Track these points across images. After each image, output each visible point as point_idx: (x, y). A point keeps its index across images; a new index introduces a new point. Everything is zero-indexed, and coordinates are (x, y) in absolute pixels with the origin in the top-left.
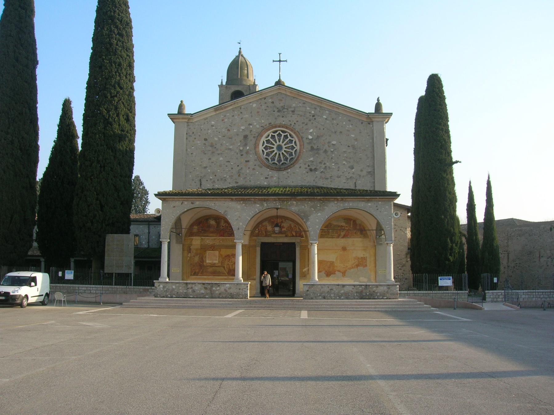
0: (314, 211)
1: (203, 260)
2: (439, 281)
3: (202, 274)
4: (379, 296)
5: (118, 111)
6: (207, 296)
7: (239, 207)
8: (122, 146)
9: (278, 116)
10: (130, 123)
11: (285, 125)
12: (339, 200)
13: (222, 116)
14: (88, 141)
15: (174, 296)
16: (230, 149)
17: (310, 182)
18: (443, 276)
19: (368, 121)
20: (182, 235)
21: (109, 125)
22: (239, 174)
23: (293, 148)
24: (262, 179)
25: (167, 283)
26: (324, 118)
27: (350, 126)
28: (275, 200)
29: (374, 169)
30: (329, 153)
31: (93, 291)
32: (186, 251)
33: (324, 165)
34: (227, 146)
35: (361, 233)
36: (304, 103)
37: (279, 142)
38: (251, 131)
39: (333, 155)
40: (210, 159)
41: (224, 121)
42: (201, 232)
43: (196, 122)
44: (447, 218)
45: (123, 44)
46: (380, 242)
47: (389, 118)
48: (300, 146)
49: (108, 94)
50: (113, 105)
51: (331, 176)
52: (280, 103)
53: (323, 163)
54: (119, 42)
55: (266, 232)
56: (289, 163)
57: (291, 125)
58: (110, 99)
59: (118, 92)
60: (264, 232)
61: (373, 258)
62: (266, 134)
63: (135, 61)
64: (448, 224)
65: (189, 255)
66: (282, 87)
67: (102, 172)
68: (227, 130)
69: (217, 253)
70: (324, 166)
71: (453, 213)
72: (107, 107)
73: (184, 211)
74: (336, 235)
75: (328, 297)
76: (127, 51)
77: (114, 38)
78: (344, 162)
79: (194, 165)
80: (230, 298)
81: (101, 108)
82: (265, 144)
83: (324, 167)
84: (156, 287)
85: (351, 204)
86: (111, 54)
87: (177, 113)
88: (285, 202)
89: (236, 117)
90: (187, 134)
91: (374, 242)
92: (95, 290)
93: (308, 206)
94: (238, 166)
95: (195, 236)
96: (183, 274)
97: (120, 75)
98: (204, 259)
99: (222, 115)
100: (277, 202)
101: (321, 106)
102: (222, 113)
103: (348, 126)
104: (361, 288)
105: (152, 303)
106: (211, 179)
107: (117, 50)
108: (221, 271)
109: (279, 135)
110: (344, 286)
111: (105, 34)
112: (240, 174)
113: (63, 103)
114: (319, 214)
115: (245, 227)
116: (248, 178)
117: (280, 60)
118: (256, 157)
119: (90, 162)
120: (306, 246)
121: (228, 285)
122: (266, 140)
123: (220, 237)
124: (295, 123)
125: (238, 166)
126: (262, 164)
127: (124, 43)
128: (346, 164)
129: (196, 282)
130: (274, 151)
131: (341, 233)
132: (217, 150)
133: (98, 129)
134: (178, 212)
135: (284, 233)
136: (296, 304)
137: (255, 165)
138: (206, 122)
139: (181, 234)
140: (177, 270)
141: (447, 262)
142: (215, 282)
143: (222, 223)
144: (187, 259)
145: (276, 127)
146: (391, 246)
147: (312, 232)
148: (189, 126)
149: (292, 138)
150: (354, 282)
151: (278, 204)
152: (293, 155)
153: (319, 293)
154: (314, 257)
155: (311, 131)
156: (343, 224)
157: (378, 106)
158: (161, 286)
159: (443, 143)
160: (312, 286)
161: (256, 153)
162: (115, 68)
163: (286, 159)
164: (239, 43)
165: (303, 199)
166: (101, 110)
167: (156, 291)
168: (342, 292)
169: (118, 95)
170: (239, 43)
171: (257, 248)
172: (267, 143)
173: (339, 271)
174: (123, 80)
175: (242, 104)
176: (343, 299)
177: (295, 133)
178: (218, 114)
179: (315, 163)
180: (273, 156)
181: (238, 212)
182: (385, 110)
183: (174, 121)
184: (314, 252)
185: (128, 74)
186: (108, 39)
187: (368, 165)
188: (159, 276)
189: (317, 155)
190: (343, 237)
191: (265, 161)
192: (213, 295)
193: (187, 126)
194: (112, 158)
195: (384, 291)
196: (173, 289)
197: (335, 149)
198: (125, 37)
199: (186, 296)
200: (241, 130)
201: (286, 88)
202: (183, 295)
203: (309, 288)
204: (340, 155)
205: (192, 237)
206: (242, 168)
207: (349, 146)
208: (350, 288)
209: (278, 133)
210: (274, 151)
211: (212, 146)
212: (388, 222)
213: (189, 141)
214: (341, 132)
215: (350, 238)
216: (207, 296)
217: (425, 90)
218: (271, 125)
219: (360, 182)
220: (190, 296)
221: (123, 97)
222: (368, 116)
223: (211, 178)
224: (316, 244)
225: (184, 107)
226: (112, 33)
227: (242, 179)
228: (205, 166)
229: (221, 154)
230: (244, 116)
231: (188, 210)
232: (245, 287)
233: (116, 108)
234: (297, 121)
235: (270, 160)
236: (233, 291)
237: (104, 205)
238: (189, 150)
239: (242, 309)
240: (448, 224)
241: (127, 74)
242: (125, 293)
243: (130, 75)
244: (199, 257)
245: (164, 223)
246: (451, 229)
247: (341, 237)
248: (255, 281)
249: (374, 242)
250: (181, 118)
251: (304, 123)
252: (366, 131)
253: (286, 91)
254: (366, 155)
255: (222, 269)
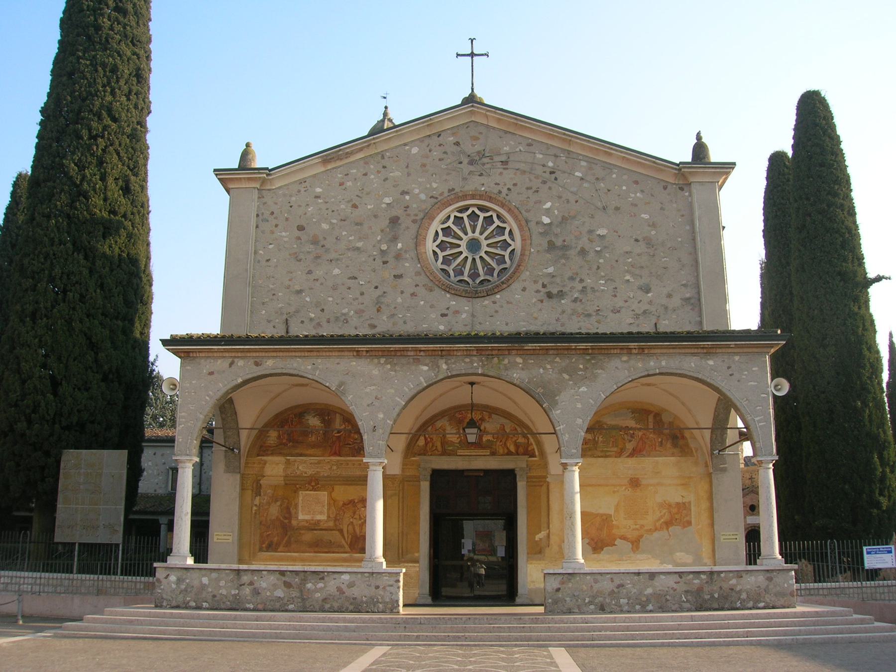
0: (569, 380)
1: (289, 513)
2: (865, 556)
3: (288, 547)
4: (744, 600)
5: (105, 170)
6: (291, 607)
7: (375, 372)
8: (110, 247)
9: (471, 173)
10: (131, 198)
11: (486, 193)
12: (634, 351)
13: (339, 176)
14: (31, 233)
15: (205, 605)
16: (358, 249)
17: (549, 324)
18: (874, 545)
19: (678, 184)
20: (239, 452)
21: (81, 198)
22: (377, 306)
23: (505, 245)
24: (434, 317)
25: (187, 569)
26: (577, 176)
27: (638, 194)
28: (468, 354)
29: (699, 293)
30: (592, 255)
31: (25, 586)
32: (250, 492)
33: (580, 284)
34: (350, 241)
35: (675, 445)
36: (529, 145)
37: (474, 232)
38: (407, 207)
39: (601, 261)
40: (310, 272)
41: (343, 187)
42: (286, 445)
43: (280, 188)
44: (867, 406)
45: (124, 28)
46: (722, 466)
47: (728, 174)
48: (522, 240)
49: (84, 131)
50: (92, 155)
51: (599, 310)
52: (473, 145)
53: (578, 279)
54: (116, 23)
55: (442, 444)
56: (498, 281)
57: (500, 192)
58: (87, 142)
59: (105, 128)
60: (439, 444)
61: (705, 505)
62: (442, 215)
63: (153, 70)
64: (871, 421)
65: (257, 501)
66: (478, 108)
67: (60, 305)
68: (350, 205)
69: (323, 495)
70: (579, 287)
71: (879, 395)
72: (80, 159)
73: (234, 383)
74: (615, 449)
75: (613, 607)
76: (134, 45)
77: (106, 16)
78: (628, 277)
79: (271, 286)
80: (351, 612)
81: (64, 161)
82: (441, 237)
83: (580, 288)
84: (159, 581)
85: (663, 363)
86: (97, 47)
87: (237, 167)
88: (496, 359)
89: (372, 177)
90: (258, 215)
91: (707, 466)
92: (31, 584)
93: (553, 369)
94: (376, 287)
95: (272, 454)
96: (241, 546)
97: (113, 93)
98: (293, 511)
99: (340, 174)
100: (475, 358)
101: (568, 150)
102: (339, 169)
103: (633, 195)
104: (696, 581)
105: (141, 623)
106: (311, 319)
107: (110, 40)
108: (333, 541)
109: (473, 217)
110: (652, 575)
111: (85, 7)
112: (382, 306)
113: (14, 181)
114: (584, 389)
115: (392, 423)
116: (401, 316)
117: (472, 52)
118: (419, 265)
119: (33, 280)
120: (540, 477)
121: (346, 577)
122: (442, 229)
123: (332, 458)
124: (509, 189)
125: (376, 287)
126: (434, 283)
127: (128, 28)
128: (632, 280)
129: (262, 567)
130: (461, 253)
131: (627, 444)
132: (327, 251)
133: (56, 206)
134: (221, 387)
135: (489, 446)
136: (531, 630)
137: (417, 285)
138: (303, 190)
139: (237, 449)
140: (227, 537)
141: (875, 511)
142: (313, 569)
143: (338, 424)
144: (252, 510)
145: (465, 197)
146: (769, 468)
147: (567, 436)
148: (263, 197)
149: (504, 222)
150: (662, 563)
151: (475, 364)
152: (506, 263)
153: (588, 597)
154: (573, 503)
155: (548, 205)
156: (632, 423)
157: (700, 150)
158: (173, 578)
159: (847, 235)
160: (570, 577)
161: (419, 258)
162: (104, 75)
163: (491, 271)
164: (385, 98)
165: (541, 352)
166: (66, 164)
167: (160, 591)
168: (649, 591)
169: (106, 133)
170: (385, 98)
171: (422, 483)
172: (443, 236)
173: (623, 538)
174: (119, 101)
175: (386, 147)
176: (651, 611)
177: (509, 211)
178: (331, 169)
179: (558, 280)
180: (458, 265)
181: (374, 385)
182: (715, 155)
183: (231, 186)
184: (573, 487)
185: (134, 92)
186: (92, 18)
187: (684, 282)
188: (169, 551)
189: (563, 261)
190: (631, 455)
191: (440, 275)
192: (307, 604)
193: (259, 198)
194: (85, 272)
195: (759, 587)
196: (203, 587)
197: (605, 247)
198: (131, 17)
199: (236, 605)
200: (384, 206)
201: (488, 111)
202: (229, 603)
203: (563, 583)
204: (617, 261)
205: (264, 458)
206: (384, 293)
207: (637, 240)
208: (671, 581)
209: (469, 212)
210: (461, 253)
211: (315, 242)
212: (759, 408)
213: (263, 232)
214: (617, 209)
215: (649, 456)
216: (291, 607)
217: (793, 127)
218: (453, 192)
219: (667, 322)
220: (248, 606)
221: (118, 139)
222: (680, 170)
223: (313, 315)
224: (577, 467)
225: (254, 156)
226: (101, 6)
227: (385, 318)
228: (297, 288)
229: (338, 260)
230: (391, 174)
231: (246, 382)
232: (390, 583)
233: (101, 163)
234: (515, 185)
235: (452, 273)
236: (360, 591)
237: (62, 379)
238: (261, 252)
239: (381, 645)
240: (871, 421)
241: (130, 92)
242: (99, 592)
243: (137, 95)
244: (281, 505)
245: (183, 414)
246: (879, 433)
247: (627, 454)
248: (418, 565)
249: (707, 466)
250: (244, 178)
251: (531, 188)
252: (675, 205)
253: (487, 116)
254: (679, 260)
255: (335, 536)
